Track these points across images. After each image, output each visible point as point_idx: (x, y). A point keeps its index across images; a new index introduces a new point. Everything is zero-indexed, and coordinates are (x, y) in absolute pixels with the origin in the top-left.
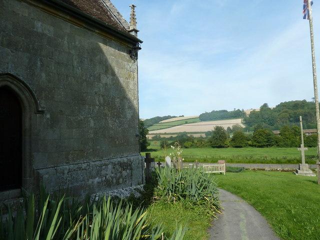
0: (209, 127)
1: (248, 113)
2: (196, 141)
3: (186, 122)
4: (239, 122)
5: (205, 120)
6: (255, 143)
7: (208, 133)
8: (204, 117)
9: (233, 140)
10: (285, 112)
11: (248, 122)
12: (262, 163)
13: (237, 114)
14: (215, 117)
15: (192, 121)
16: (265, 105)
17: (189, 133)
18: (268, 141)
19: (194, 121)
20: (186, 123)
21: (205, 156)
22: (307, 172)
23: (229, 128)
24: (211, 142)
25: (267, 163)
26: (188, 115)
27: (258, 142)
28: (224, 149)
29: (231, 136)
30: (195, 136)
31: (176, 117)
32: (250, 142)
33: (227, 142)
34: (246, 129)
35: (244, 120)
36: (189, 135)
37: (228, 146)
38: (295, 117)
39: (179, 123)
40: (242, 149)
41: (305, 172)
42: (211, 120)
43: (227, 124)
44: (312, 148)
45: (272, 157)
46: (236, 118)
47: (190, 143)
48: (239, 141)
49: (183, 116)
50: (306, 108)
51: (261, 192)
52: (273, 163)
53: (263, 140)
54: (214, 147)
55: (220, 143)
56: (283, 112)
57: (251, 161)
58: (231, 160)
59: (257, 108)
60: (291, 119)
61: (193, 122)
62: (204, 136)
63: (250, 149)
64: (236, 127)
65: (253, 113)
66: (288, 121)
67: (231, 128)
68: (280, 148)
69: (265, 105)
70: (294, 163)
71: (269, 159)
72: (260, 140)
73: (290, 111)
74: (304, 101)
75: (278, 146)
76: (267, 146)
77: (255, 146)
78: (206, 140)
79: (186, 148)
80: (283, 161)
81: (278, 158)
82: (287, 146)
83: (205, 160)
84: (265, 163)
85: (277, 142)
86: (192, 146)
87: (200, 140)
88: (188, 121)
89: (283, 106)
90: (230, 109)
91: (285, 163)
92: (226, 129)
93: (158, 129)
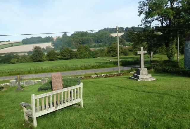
0: (31, 48)
1: (55, 39)
2: (20, 58)
3: (12, 45)
4: (49, 44)
5: (26, 44)
6: (62, 57)
7: (29, 52)
8: (26, 42)
9: (48, 55)
10: (77, 38)
11: (54, 44)
12: (75, 70)
13: (48, 40)
14: (33, 42)
15: (16, 44)
16: (65, 34)
17: (15, 53)
18: (71, 55)
19: (18, 44)
20: (12, 46)
21: (29, 69)
22: (147, 77)
23: (43, 49)
24: (32, 58)
25: (78, 70)
26: (13, 40)
27: (64, 56)
28: (42, 62)
29: (46, 54)
30: (20, 54)
31: (3, 42)
32: (59, 57)
33: (44, 57)
34: (55, 49)
35: (52, 44)
36: (15, 54)
37: (45, 60)
38: (82, 41)
39: (7, 46)
40: (54, 61)
41: (146, 76)
42: (30, 43)
43: (43, 46)
44: (95, 58)
45: (82, 65)
46: (48, 42)
47: (15, 60)
48: (51, 56)
49: (9, 41)
50: (87, 36)
51: (138, 107)
52: (82, 69)
53: (66, 55)
54: (34, 62)
55: (39, 58)
56: (76, 38)
57: (67, 69)
58: (51, 69)
59: (61, 36)
60: (80, 43)
61: (18, 45)
62: (26, 54)
63: (60, 61)
64: (48, 48)
65: (58, 38)
66: (78, 44)
67: (45, 48)
68: (78, 59)
69: (65, 34)
70: (96, 68)
71: (79, 66)
72: (66, 55)
73: (79, 38)
74: (86, 32)
75: (77, 58)
76: (70, 59)
77: (62, 59)
78: (28, 57)
79: (13, 63)
80: (89, 67)
81: (85, 65)
82: (81, 58)
83: (75, 81)
84: (76, 70)
85: (76, 56)
86: (17, 62)
87: (24, 57)
88: (14, 44)
89: (75, 35)
90: (43, 36)
91: (90, 68)
92: (42, 48)
93: (8, 47)
